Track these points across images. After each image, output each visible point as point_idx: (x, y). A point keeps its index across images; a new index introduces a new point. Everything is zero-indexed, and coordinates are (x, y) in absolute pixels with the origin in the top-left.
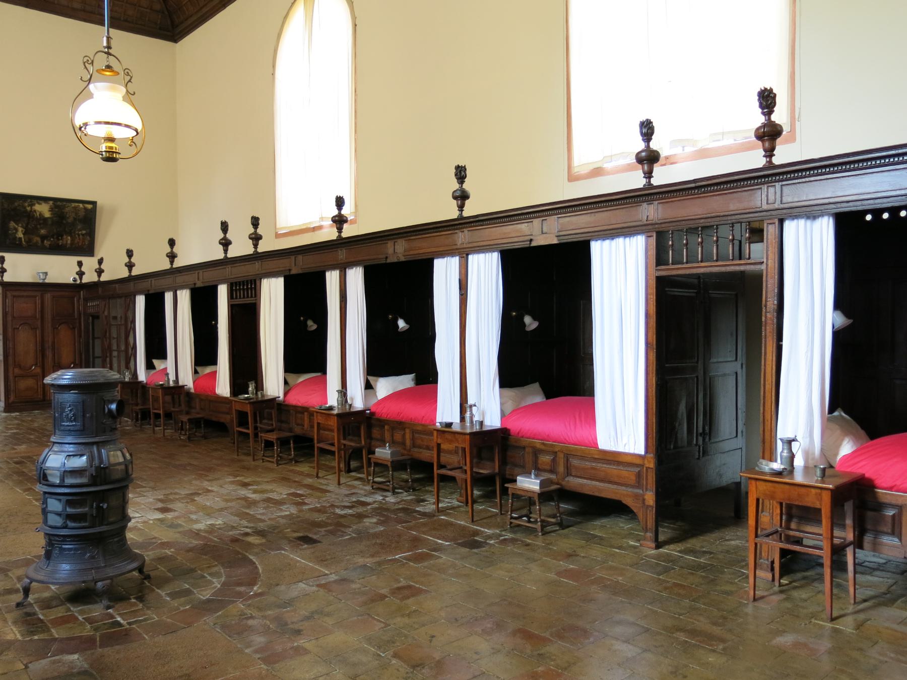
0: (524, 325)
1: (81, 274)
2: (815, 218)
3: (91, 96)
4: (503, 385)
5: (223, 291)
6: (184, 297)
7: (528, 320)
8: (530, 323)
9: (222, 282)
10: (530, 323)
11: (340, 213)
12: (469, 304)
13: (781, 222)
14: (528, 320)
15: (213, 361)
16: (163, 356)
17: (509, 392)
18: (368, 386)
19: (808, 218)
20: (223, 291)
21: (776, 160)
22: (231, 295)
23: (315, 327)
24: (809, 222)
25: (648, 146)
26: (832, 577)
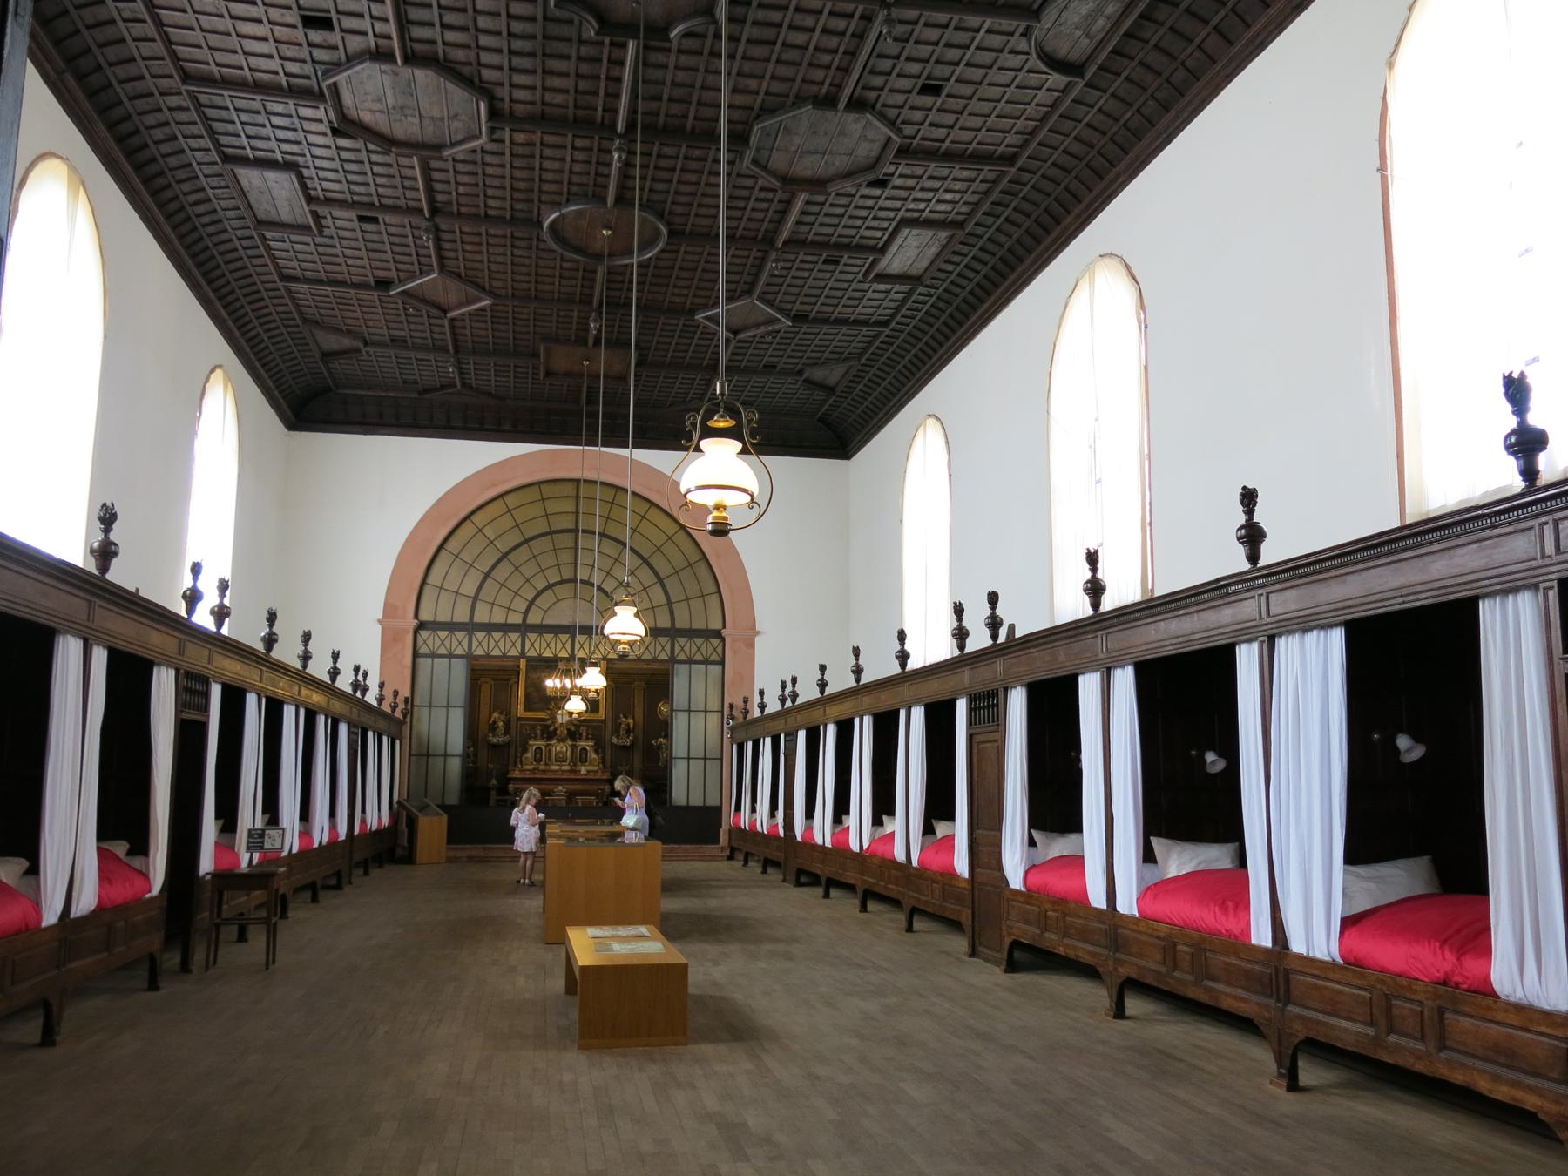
0: (1397, 751)
1: (961, 635)
2: (1306, 630)
3: (614, 614)
4: (1353, 856)
5: (962, 706)
6: (918, 714)
7: (1403, 742)
8: (1408, 748)
9: (961, 695)
10: (1408, 748)
11: (1094, 576)
12: (1297, 724)
13: (1006, 690)
14: (1403, 742)
15: (950, 816)
16: (891, 812)
17: (1360, 870)
18: (1148, 856)
19: (1322, 627)
20: (962, 706)
21: (1102, 609)
22: (971, 710)
23: (1221, 765)
24: (1322, 633)
25: (1094, 576)
26: (1130, 954)
